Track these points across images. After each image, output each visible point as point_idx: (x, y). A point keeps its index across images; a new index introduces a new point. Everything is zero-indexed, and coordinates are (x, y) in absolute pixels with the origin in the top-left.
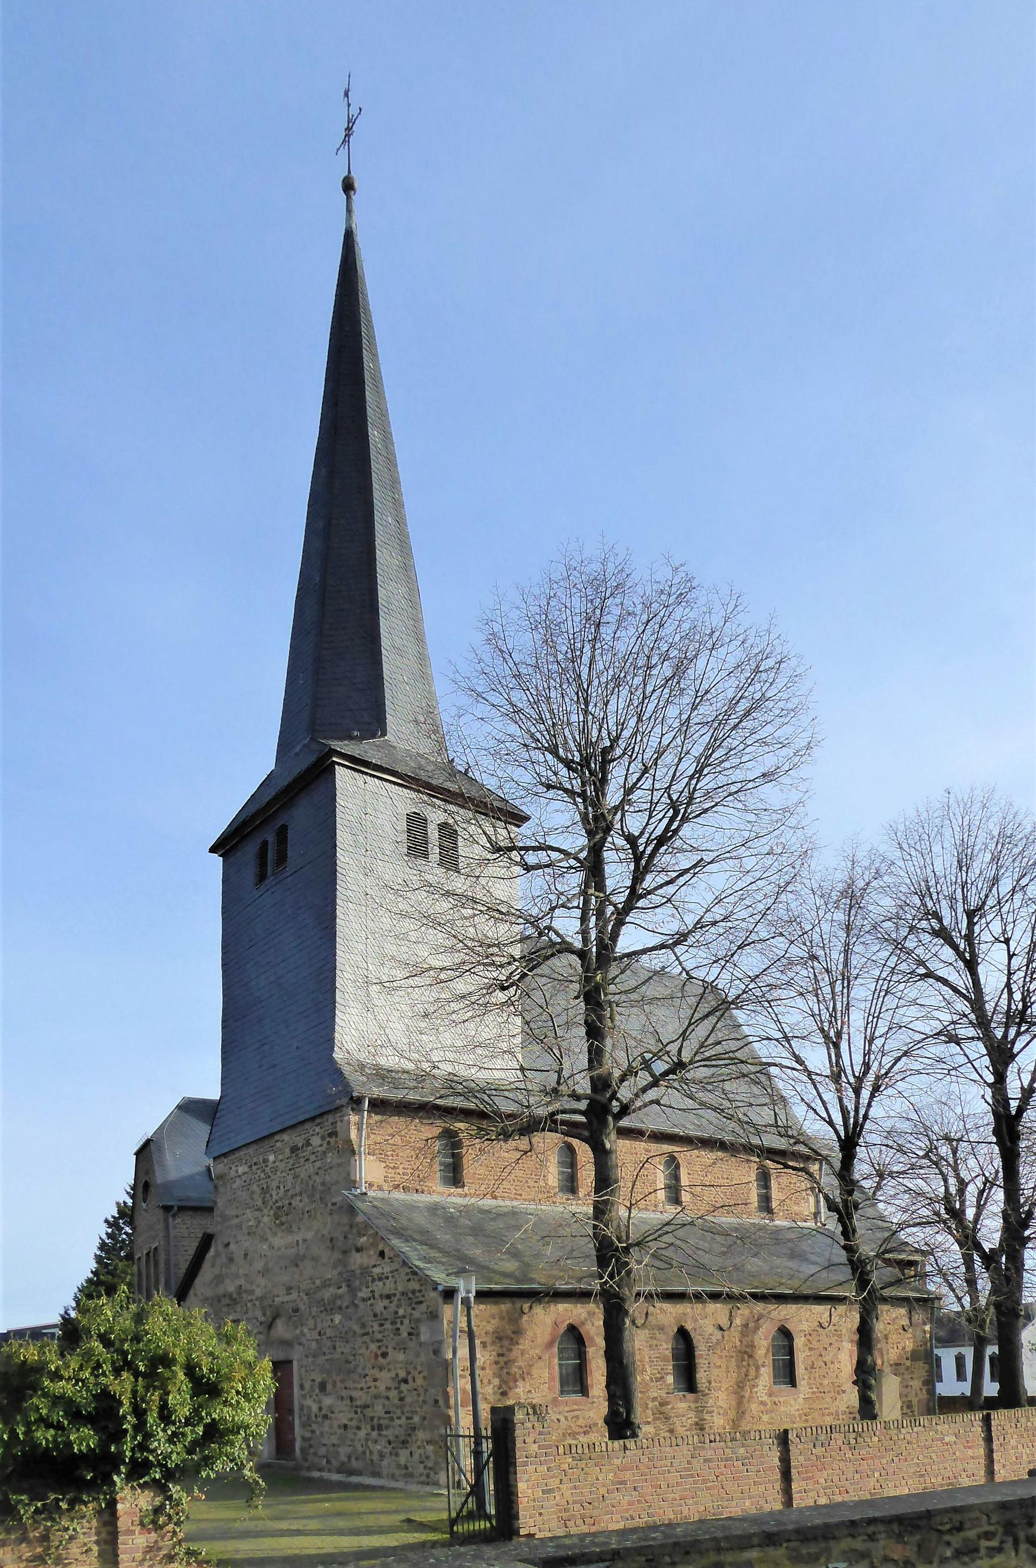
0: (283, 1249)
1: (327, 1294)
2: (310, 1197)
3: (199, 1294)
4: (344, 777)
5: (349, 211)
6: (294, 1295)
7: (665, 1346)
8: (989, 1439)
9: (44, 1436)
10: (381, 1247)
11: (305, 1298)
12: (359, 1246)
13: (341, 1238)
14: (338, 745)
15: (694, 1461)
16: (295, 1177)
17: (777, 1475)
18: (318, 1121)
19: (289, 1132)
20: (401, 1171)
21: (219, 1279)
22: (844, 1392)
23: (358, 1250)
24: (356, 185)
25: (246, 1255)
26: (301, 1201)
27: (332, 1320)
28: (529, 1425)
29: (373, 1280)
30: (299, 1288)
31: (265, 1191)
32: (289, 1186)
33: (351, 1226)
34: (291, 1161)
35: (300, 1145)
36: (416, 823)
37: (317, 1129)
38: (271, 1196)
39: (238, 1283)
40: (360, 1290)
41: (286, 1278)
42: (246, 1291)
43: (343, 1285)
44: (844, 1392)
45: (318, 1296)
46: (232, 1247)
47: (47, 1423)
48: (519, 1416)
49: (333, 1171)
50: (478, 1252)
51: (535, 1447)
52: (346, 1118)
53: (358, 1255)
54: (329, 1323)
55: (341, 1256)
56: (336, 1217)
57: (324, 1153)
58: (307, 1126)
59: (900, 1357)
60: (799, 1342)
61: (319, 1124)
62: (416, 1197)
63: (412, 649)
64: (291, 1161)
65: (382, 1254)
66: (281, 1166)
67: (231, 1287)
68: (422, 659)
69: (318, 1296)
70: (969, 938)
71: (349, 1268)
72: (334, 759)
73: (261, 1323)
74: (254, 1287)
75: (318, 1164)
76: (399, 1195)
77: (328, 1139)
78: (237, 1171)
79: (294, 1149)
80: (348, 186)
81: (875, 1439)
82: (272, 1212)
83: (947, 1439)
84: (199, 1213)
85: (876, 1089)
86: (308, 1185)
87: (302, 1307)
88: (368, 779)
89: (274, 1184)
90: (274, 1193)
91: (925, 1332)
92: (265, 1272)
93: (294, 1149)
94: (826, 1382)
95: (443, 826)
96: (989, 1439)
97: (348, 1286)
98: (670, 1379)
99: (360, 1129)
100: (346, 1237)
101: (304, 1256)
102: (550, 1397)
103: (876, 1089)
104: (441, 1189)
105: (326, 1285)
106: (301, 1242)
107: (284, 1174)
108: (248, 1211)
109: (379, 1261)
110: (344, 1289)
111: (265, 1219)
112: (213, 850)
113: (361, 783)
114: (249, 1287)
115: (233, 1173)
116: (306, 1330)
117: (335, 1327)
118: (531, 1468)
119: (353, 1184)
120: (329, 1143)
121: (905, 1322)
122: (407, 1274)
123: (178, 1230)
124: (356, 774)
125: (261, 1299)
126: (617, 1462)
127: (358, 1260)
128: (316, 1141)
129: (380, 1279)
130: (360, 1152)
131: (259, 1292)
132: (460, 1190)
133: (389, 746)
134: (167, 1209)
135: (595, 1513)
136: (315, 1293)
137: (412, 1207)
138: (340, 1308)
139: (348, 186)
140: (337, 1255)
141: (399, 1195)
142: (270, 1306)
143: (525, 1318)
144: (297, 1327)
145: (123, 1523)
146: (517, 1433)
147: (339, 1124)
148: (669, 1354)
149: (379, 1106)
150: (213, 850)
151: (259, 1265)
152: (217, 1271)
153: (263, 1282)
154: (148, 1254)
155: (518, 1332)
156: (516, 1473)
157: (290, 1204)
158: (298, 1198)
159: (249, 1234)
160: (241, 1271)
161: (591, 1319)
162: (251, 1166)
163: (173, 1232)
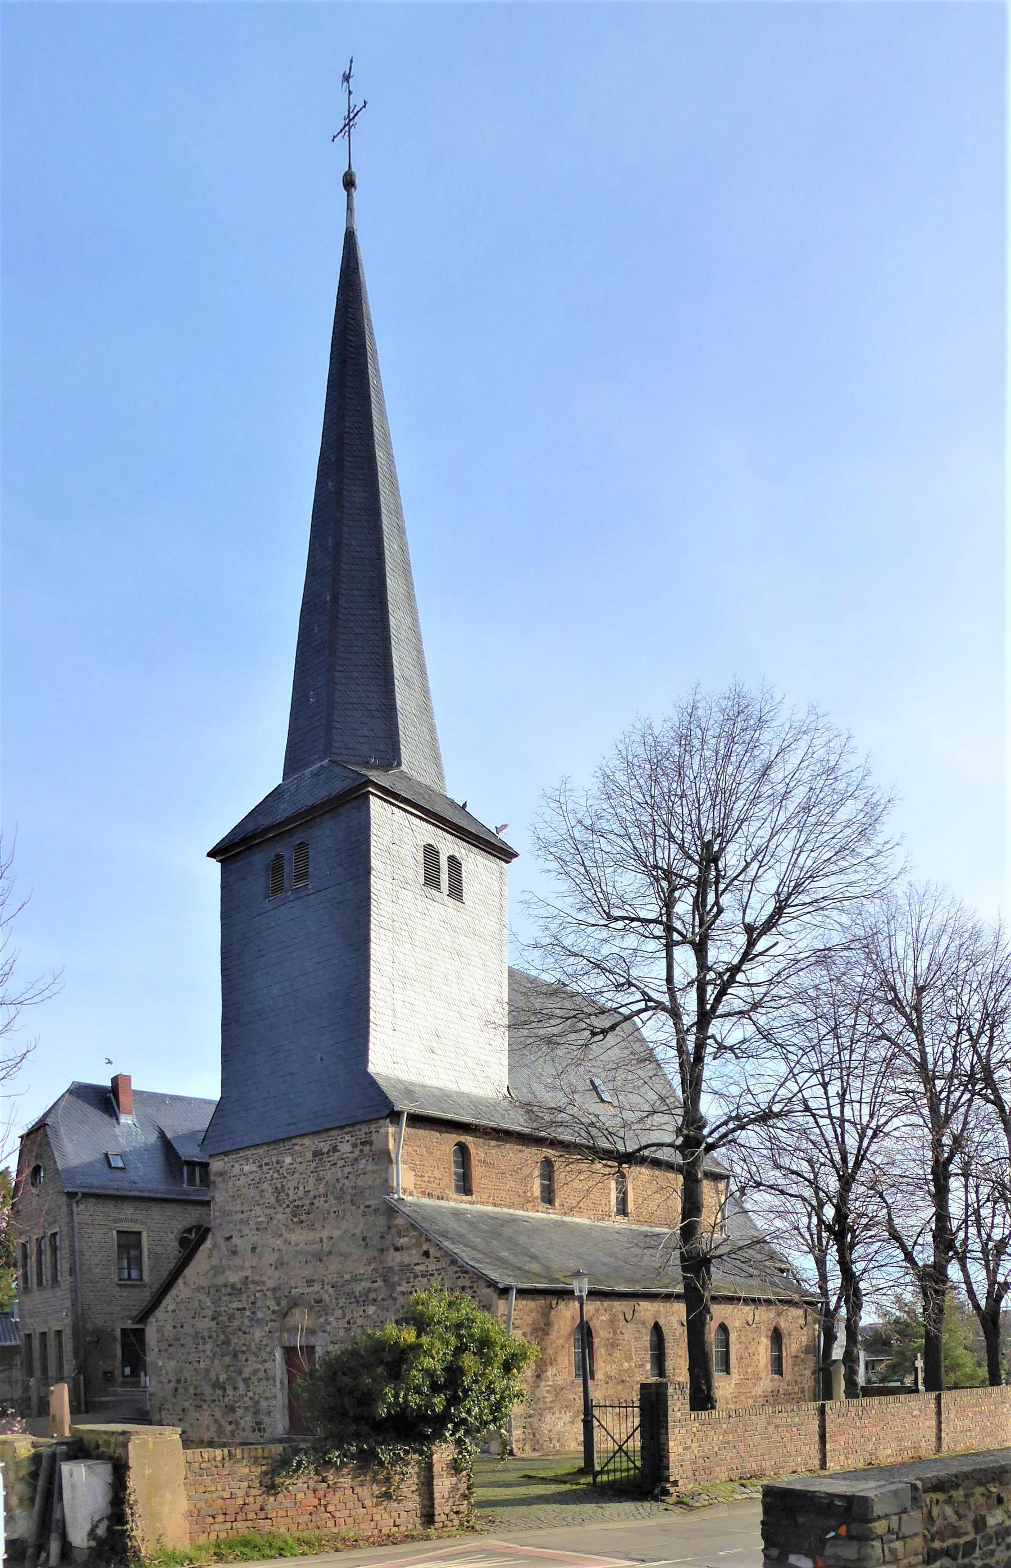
0: (301, 1245)
1: (358, 1288)
2: (338, 1199)
3: (191, 1283)
4: (377, 808)
5: (350, 208)
6: (317, 1287)
7: (645, 1338)
8: (939, 1414)
9: (414, 1400)
10: (425, 1247)
11: (331, 1290)
12: (399, 1245)
13: (377, 1238)
14: (375, 776)
15: (769, 1427)
16: (319, 1179)
17: (817, 1438)
18: (347, 1129)
19: (310, 1137)
20: (426, 1179)
21: (218, 1270)
22: (761, 1379)
23: (397, 1249)
24: (357, 182)
25: (253, 1249)
26: (326, 1202)
27: (364, 1311)
28: (676, 1397)
29: (416, 1276)
30: (323, 1281)
31: (278, 1191)
32: (310, 1187)
33: (389, 1228)
34: (314, 1164)
35: (325, 1150)
36: (431, 853)
37: (347, 1138)
38: (288, 1195)
39: (242, 1274)
40: (400, 1285)
41: (308, 1272)
42: (253, 1282)
43: (379, 1280)
44: (761, 1379)
45: (347, 1288)
46: (235, 1240)
47: (418, 1391)
48: (671, 1390)
49: (367, 1176)
50: (506, 1254)
51: (679, 1414)
52: (382, 1130)
53: (398, 1254)
54: (362, 1313)
55: (375, 1254)
56: (371, 1219)
57: (356, 1160)
58: (333, 1133)
59: (798, 1352)
60: (733, 1337)
61: (350, 1132)
62: (438, 1202)
63: (417, 682)
64: (314, 1164)
65: (426, 1254)
66: (300, 1168)
67: (234, 1278)
68: (425, 691)
69: (347, 1288)
70: (917, 1008)
71: (384, 1265)
72: (370, 789)
73: (274, 1312)
74: (264, 1278)
75: (347, 1169)
76: (425, 1201)
77: (360, 1147)
78: (242, 1170)
79: (317, 1154)
80: (349, 183)
81: (873, 1412)
82: (288, 1210)
83: (915, 1413)
84: (101, 1201)
85: (875, 1135)
86: (334, 1187)
87: (326, 1298)
88: (396, 810)
89: (291, 1185)
90: (291, 1192)
91: (814, 1330)
92: (280, 1264)
93: (317, 1154)
94: (749, 1370)
95: (452, 859)
96: (939, 1414)
97: (385, 1281)
98: (648, 1366)
99: (397, 1141)
100: (382, 1237)
101: (330, 1253)
102: (569, 1381)
103: (875, 1135)
104: (455, 1196)
105: (355, 1279)
106: (325, 1240)
107: (303, 1176)
108: (257, 1208)
109: (424, 1259)
110: (380, 1283)
111: (280, 1216)
112: (211, 854)
113: (389, 814)
114: (257, 1278)
115: (236, 1171)
116: (331, 1319)
117: (368, 1317)
118: (676, 1431)
119: (390, 1190)
120: (361, 1151)
121: (802, 1322)
122: (456, 1272)
123: (81, 1217)
124: (385, 804)
125: (274, 1290)
126: (725, 1426)
127: (394, 1259)
128: (345, 1148)
129: (423, 1276)
130: (397, 1161)
131: (270, 1284)
132: (468, 1198)
133: (404, 776)
134: (71, 1195)
135: (711, 1465)
136: (342, 1286)
137: (439, 1210)
138: (375, 1300)
139: (349, 183)
140: (372, 1253)
141: (425, 1201)
142: (286, 1297)
143: (553, 1313)
144: (321, 1316)
145: (437, 1469)
146: (669, 1403)
147: (374, 1135)
148: (648, 1344)
149: (417, 1120)
150: (211, 854)
151: (273, 1258)
152: (214, 1261)
153: (276, 1274)
154: (39, 1241)
155: (548, 1324)
156: (667, 1434)
157: (312, 1204)
158: (322, 1199)
159: (258, 1229)
160: (247, 1264)
161: (674, 1317)
162: (261, 1166)
163: (77, 1219)
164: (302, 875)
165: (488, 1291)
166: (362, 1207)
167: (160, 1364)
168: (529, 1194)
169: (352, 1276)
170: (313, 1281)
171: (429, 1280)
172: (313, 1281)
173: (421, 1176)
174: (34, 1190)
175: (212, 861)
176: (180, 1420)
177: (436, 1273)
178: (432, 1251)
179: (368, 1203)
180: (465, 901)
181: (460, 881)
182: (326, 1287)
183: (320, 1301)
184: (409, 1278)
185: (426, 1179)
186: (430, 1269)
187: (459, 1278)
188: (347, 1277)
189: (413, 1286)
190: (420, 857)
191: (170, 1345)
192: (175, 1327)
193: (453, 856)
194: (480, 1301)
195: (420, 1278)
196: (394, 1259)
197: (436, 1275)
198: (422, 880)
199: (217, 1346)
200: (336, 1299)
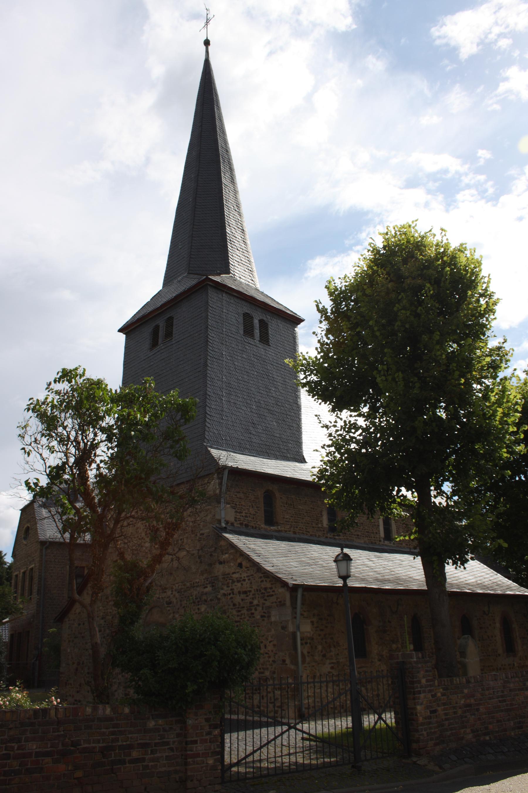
10: (239, 561)
11: (177, 595)
12: (222, 560)
20: (244, 514)
23: (221, 563)
27: (198, 609)
29: (233, 582)
30: (172, 588)
40: (222, 589)
43: (208, 586)
54: (197, 611)
65: (240, 565)
87: (174, 600)
95: (261, 321)
97: (213, 586)
112: (120, 331)
116: (177, 616)
122: (261, 577)
129: (238, 581)
138: (206, 601)
150: (120, 331)
154: (24, 573)
164: (169, 334)
165: (281, 590)
166: (198, 535)
167: (69, 651)
168: (320, 525)
169: (191, 584)
170: (166, 589)
171: (242, 584)
172: (166, 589)
173: (240, 513)
174: (25, 542)
175: (121, 334)
176: (78, 692)
177: (246, 578)
178: (244, 563)
179: (201, 532)
180: (271, 344)
181: (267, 334)
182: (174, 592)
183: (170, 603)
184: (228, 583)
185: (244, 514)
186: (242, 576)
187: (262, 581)
188: (188, 584)
189: (232, 589)
190: (241, 320)
191: (75, 638)
192: (79, 624)
193: (263, 320)
194: (277, 598)
195: (236, 584)
196: (219, 570)
197: (247, 581)
198: (242, 332)
199: (104, 637)
200: (181, 601)
